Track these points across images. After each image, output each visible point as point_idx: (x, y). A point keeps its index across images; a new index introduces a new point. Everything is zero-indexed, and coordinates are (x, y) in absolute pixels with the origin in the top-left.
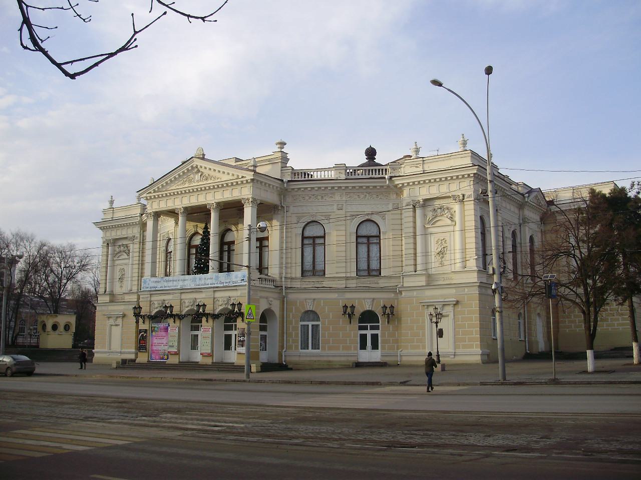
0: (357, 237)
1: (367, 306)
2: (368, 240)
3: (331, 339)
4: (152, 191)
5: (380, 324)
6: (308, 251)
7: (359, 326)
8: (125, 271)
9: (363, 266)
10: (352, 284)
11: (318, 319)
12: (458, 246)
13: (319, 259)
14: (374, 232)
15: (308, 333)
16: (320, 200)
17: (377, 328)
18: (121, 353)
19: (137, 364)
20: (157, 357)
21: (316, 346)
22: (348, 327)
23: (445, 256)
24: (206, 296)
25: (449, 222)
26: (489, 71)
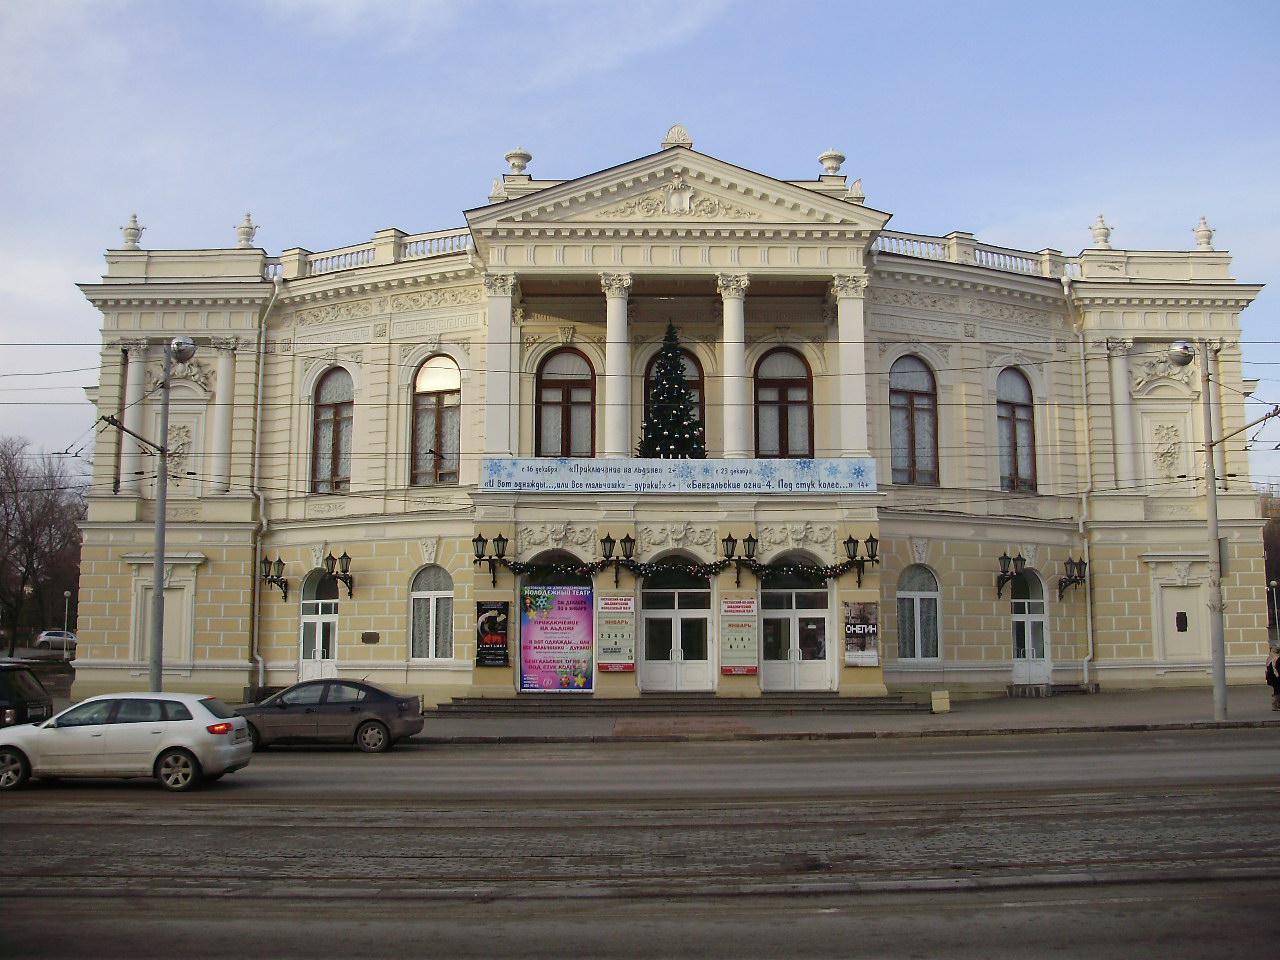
3: (964, 632)
4: (517, 215)
8: (191, 434)
10: (998, 508)
11: (449, 587)
12: (216, 444)
14: (921, 383)
16: (930, 308)
18: (193, 669)
19: (597, 703)
20: (548, 681)
21: (931, 650)
22: (994, 605)
23: (185, 462)
25: (201, 394)
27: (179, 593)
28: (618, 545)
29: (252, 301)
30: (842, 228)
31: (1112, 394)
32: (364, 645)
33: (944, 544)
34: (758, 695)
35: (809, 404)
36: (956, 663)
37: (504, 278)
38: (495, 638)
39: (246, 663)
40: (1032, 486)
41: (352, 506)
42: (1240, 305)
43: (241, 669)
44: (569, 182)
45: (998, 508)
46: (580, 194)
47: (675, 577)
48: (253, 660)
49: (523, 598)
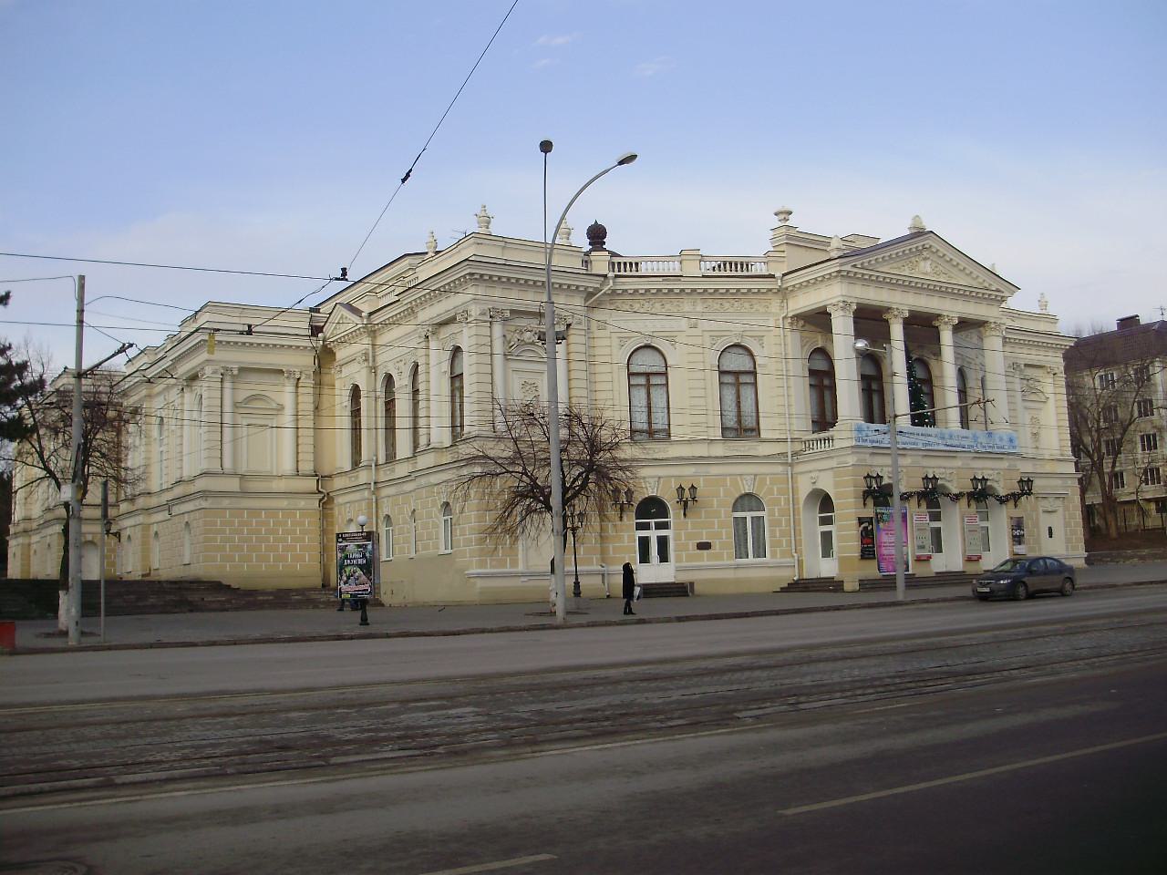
0: (630, 375)
1: (747, 487)
2: (648, 380)
7: (820, 517)
10: (719, 450)
13: (747, 406)
14: (745, 364)
17: (665, 526)
24: (858, 460)
26: (546, 147)
30: (997, 293)
33: (728, 480)
45: (719, 450)
49: (877, 514)
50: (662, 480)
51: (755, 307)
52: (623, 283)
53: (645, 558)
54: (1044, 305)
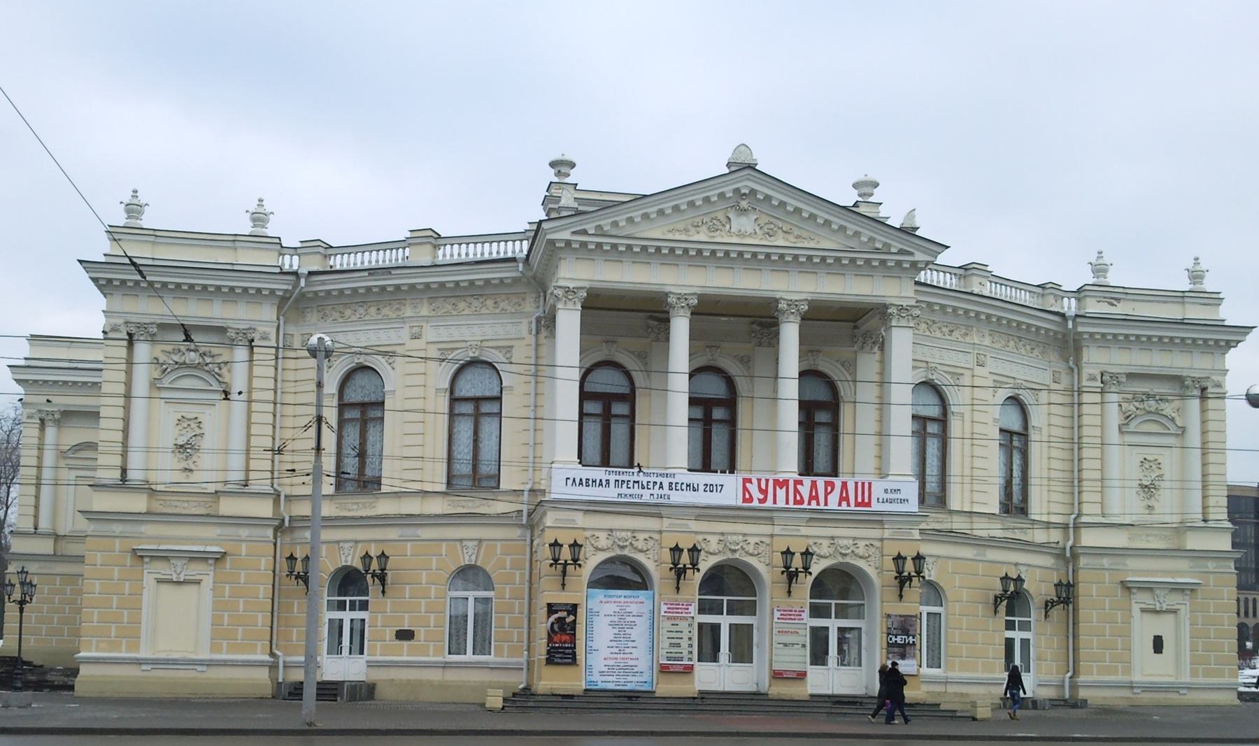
2: (477, 408)
5: (809, 601)
6: (465, 430)
9: (464, 468)
10: (437, 506)
13: (487, 452)
15: (474, 636)
17: (750, 609)
21: (935, 662)
27: (194, 588)
28: (566, 548)
29: (272, 291)
31: (249, 412)
32: (398, 642)
34: (808, 698)
35: (631, 417)
36: (955, 674)
37: (574, 291)
38: (564, 638)
39: (267, 658)
40: (1023, 511)
41: (385, 507)
42: (1229, 345)
43: (260, 664)
44: (645, 196)
46: (652, 210)
47: (729, 583)
48: (272, 654)
50: (484, 544)
51: (502, 305)
52: (323, 283)
53: (819, 656)
54: (1196, 276)
